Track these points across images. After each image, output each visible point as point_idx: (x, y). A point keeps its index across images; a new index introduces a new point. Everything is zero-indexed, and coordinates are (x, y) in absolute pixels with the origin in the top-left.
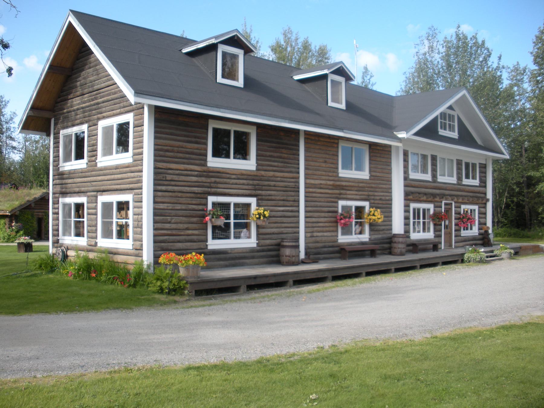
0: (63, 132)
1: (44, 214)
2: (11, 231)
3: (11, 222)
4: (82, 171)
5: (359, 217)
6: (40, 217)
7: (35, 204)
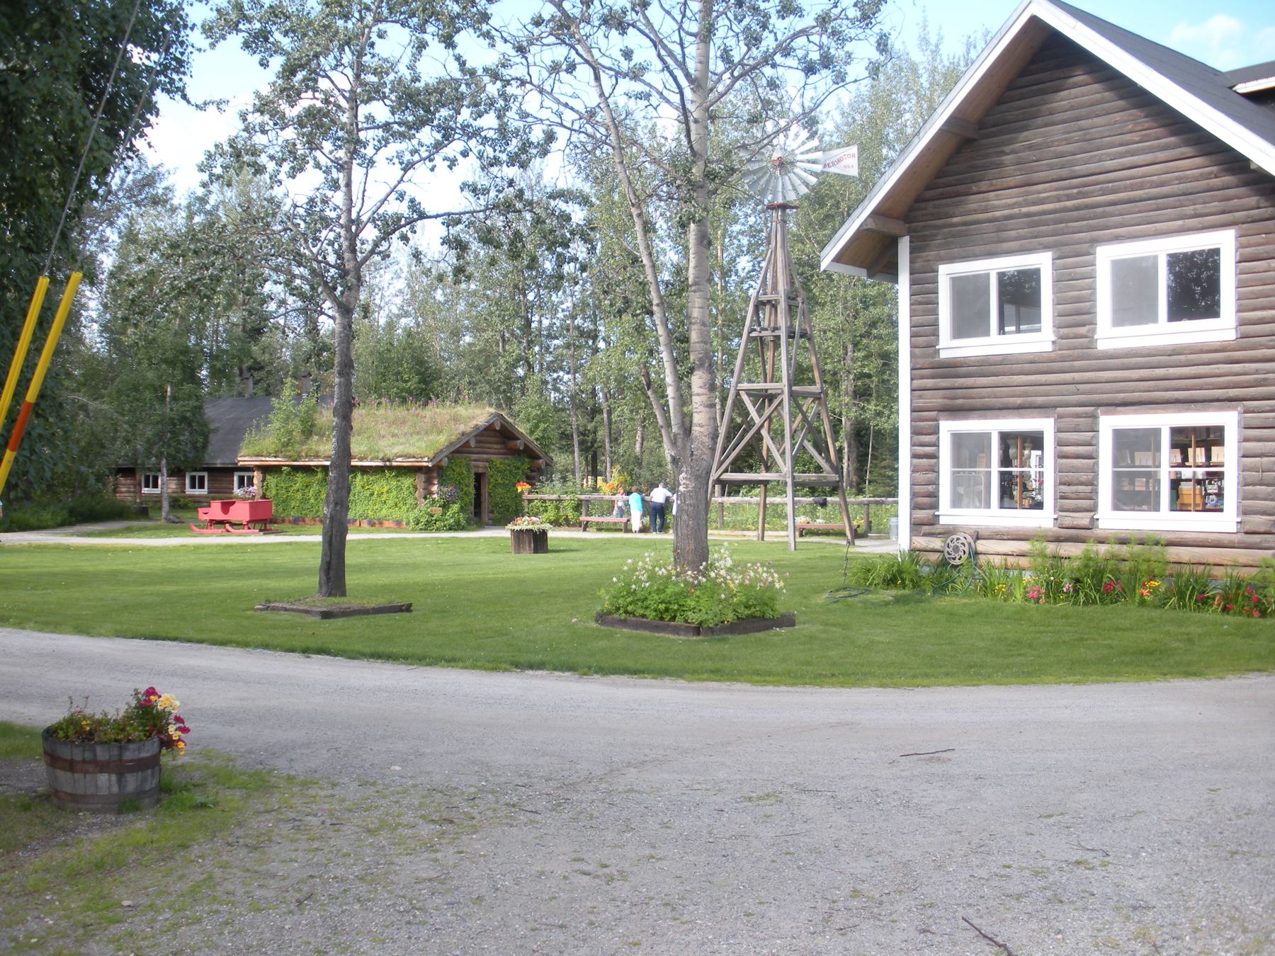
0: (946, 273)
1: (487, 464)
2: (432, 505)
3: (429, 482)
4: (1032, 364)
5: (965, 454)
6: (480, 471)
7: (478, 442)
